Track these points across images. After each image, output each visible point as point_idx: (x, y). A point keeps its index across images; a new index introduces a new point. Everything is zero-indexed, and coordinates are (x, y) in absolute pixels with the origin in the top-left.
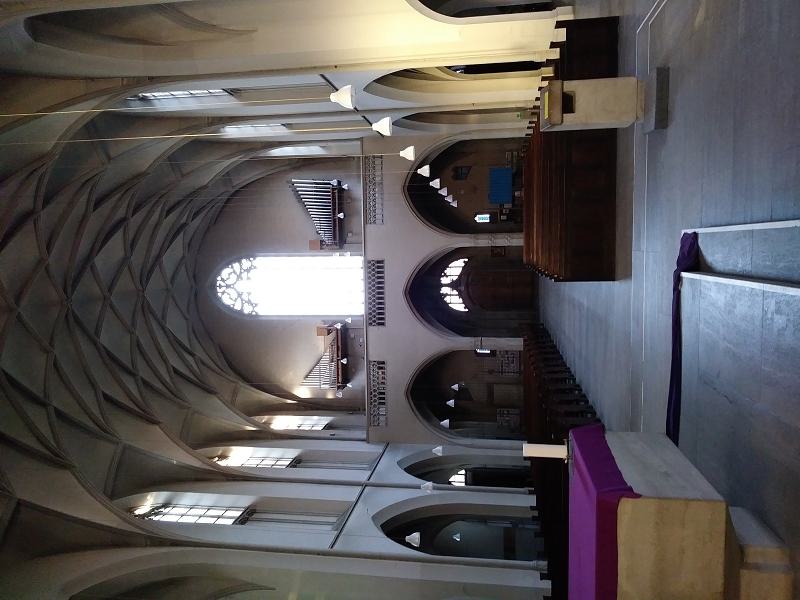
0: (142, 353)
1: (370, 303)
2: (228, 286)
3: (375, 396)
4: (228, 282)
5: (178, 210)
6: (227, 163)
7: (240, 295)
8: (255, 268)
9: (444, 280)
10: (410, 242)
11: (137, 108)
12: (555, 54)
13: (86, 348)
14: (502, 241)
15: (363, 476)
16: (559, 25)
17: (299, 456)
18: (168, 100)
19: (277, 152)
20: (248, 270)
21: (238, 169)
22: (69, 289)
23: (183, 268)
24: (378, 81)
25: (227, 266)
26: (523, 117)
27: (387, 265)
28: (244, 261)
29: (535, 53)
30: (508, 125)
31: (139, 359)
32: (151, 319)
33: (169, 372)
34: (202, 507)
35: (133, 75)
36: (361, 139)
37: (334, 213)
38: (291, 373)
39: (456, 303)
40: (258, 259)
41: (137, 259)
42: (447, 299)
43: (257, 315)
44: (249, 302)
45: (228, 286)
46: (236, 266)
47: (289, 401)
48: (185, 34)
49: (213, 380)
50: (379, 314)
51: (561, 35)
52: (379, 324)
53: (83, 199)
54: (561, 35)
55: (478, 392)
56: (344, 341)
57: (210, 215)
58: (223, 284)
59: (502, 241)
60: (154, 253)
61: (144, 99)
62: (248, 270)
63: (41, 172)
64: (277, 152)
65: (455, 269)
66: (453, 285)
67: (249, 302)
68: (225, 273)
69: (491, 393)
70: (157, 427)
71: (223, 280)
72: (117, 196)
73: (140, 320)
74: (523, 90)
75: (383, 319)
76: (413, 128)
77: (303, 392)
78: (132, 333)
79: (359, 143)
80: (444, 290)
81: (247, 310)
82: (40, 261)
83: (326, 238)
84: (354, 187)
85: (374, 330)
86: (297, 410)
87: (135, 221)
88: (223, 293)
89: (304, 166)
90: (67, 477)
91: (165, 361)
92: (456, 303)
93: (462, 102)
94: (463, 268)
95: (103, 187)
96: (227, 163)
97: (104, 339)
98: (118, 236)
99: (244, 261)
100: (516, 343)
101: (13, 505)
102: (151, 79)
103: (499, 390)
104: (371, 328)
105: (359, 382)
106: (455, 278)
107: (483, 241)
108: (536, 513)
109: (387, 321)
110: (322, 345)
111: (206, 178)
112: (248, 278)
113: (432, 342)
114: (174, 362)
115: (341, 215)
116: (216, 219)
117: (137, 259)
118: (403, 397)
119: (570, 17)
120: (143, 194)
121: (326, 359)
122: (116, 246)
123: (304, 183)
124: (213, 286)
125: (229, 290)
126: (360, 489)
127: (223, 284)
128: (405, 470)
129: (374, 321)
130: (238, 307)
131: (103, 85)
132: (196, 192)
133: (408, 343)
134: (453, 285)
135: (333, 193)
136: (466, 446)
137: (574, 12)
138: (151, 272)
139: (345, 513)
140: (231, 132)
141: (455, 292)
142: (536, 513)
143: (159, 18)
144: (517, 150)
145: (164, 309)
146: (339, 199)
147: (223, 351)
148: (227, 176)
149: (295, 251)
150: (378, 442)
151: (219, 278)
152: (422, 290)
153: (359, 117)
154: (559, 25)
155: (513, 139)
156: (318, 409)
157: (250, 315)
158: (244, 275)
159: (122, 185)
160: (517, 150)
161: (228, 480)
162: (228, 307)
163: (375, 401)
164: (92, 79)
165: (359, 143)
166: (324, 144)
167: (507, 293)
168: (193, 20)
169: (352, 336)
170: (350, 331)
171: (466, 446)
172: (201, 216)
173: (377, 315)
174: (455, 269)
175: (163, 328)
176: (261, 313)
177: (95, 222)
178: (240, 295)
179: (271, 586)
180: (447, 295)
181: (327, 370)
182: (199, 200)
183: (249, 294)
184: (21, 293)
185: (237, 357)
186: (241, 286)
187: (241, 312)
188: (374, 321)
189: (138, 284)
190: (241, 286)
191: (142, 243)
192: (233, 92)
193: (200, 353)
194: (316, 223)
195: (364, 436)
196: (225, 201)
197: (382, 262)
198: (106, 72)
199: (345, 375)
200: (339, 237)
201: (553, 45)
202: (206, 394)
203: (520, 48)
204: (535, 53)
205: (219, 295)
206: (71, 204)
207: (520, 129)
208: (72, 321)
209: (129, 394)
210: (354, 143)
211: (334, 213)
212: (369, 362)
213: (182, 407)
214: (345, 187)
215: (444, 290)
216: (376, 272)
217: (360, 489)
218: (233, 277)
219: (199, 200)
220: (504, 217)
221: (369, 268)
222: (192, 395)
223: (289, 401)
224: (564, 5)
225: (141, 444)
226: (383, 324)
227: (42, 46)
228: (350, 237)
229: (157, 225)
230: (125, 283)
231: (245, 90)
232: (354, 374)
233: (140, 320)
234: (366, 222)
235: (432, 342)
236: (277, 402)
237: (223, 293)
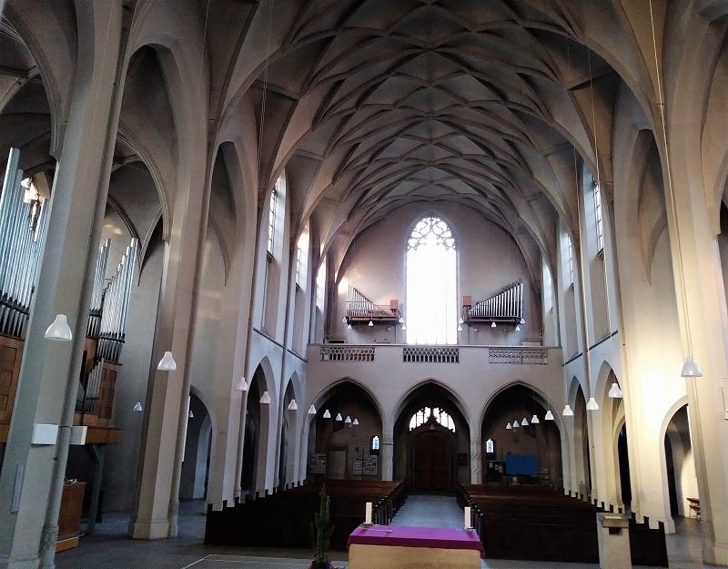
0: (386, 165)
1: (426, 350)
2: (431, 227)
3: (337, 351)
4: (435, 227)
5: (500, 195)
6: (538, 234)
7: (424, 236)
8: (447, 249)
9: (436, 411)
10: (475, 384)
11: (587, 179)
12: (640, 521)
13: (394, 130)
14: (475, 465)
15: (289, 347)
16: (661, 524)
17: (302, 291)
18: (593, 202)
19: (546, 272)
20: (445, 244)
21: (531, 238)
22: (444, 119)
23: (448, 193)
24: (612, 371)
25: (449, 226)
26: (581, 486)
27: (454, 365)
28: (453, 240)
29: (638, 502)
30: (574, 474)
31: (378, 165)
32: (407, 173)
33: (369, 185)
34: (274, 221)
35: (615, 188)
36: (560, 347)
37: (496, 318)
38: (359, 277)
39: (417, 420)
40: (455, 252)
41: (459, 162)
42: (420, 413)
43: (407, 250)
44: (418, 244)
45: (431, 227)
46: (449, 234)
47: (336, 275)
48: (646, 233)
49: (357, 217)
50: (413, 357)
51: (654, 525)
52: (405, 357)
53: (510, 132)
54: (654, 525)
55: (339, 438)
56: (387, 322)
57: (493, 215)
58: (434, 222)
59: (475, 465)
60: (471, 128)
61: (594, 185)
62: (445, 244)
63: (537, 110)
64: (546, 272)
65: (446, 421)
66: (432, 419)
67: (418, 244)
68: (443, 225)
69: (339, 449)
70: (331, 181)
71: (437, 222)
72: (513, 154)
73: (408, 164)
74: (606, 489)
75: (409, 360)
76: (571, 392)
77: (344, 287)
78: (395, 105)
79: (557, 345)
80: (428, 410)
81: (412, 242)
82: (466, 101)
83: (474, 311)
84: (514, 339)
85: (399, 353)
86: (329, 283)
87: (492, 164)
88: (426, 223)
89: (535, 297)
90: (308, 125)
91: (376, 182)
92: (417, 420)
93: (595, 436)
94: (447, 428)
95: (523, 147)
96: (538, 234)
97: (399, 141)
98: (480, 151)
99: (453, 240)
100: (388, 475)
101: (294, 96)
102: (612, 204)
103: (340, 456)
104: (402, 349)
105: (353, 337)
106: (438, 421)
107: (475, 449)
108: (290, 487)
109: (407, 364)
110: (382, 303)
111: (525, 216)
112: (438, 244)
113: (389, 405)
114: (376, 188)
115: (494, 325)
116: (488, 219)
117: (459, 162)
118: (344, 375)
119: (667, 531)
120: (515, 172)
121: (371, 308)
122: (469, 148)
123: (520, 293)
124: (432, 215)
125: (428, 227)
126: (281, 343)
127: (434, 222)
128: (260, 365)
129: (407, 353)
130: (414, 234)
131: (606, 166)
132: (512, 206)
133: (389, 382)
134: (432, 419)
135: (511, 318)
136: (303, 429)
137: (670, 535)
138: (448, 171)
139: (266, 333)
140: (565, 243)
141: (426, 420)
142: (290, 487)
143: (658, 214)
144: (549, 479)
145: (418, 180)
146: (507, 323)
147: (377, 223)
148: (524, 230)
149: (462, 283)
150: (308, 353)
151: (438, 220)
152: (431, 394)
153: (581, 350)
154: (661, 524)
155: (561, 476)
156: (291, 215)
157: (407, 244)
158: (441, 240)
159: (522, 157)
160: (549, 479)
161: (291, 238)
162: (414, 227)
163: (337, 351)
164: (611, 159)
165: (557, 345)
166: (554, 311)
167: (431, 466)
168: (657, 239)
169: (389, 329)
170: (393, 327)
171: (303, 429)
172: (493, 209)
173: (413, 355)
174: (446, 421)
175: (397, 134)
176: (409, 253)
177: (491, 137)
178: (424, 236)
179: (229, 280)
180: (423, 411)
181: (361, 308)
182: (508, 212)
183: (425, 244)
184: (443, 89)
185: (377, 231)
186: (432, 238)
187: (410, 237)
188: (407, 353)
189: (440, 162)
190: (432, 237)
191: (472, 166)
192: (600, 255)
193: (379, 206)
194: (486, 302)
195: (312, 342)
196: (503, 225)
197: (457, 361)
198: (616, 174)
199: (358, 323)
200: (475, 321)
201: (646, 519)
202: (348, 213)
203: (641, 496)
204: (638, 502)
205: (425, 220)
206: (511, 126)
207: (570, 484)
208: (415, 120)
209: (342, 100)
210: (557, 342)
211: (496, 318)
212: (373, 347)
213: (342, 197)
214: (518, 328)
215: (428, 410)
216: (448, 355)
217: (281, 343)
218: (439, 232)
219: (508, 212)
220: (491, 465)
221: (444, 350)
222: (348, 204)
223: (336, 275)
224: (676, 526)
225: (320, 175)
226: (405, 360)
227: (635, 136)
228: (473, 330)
229: (488, 179)
230: (441, 154)
231: (603, 264)
232: (357, 329)
233: (408, 164)
234: (490, 348)
235: (389, 405)
236: (336, 264)
237: (426, 223)
